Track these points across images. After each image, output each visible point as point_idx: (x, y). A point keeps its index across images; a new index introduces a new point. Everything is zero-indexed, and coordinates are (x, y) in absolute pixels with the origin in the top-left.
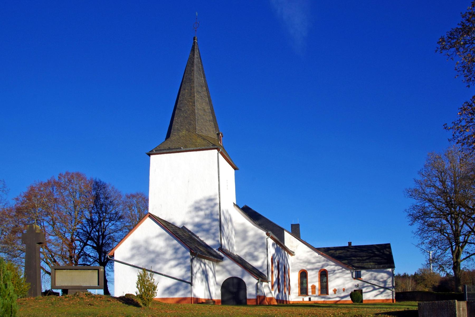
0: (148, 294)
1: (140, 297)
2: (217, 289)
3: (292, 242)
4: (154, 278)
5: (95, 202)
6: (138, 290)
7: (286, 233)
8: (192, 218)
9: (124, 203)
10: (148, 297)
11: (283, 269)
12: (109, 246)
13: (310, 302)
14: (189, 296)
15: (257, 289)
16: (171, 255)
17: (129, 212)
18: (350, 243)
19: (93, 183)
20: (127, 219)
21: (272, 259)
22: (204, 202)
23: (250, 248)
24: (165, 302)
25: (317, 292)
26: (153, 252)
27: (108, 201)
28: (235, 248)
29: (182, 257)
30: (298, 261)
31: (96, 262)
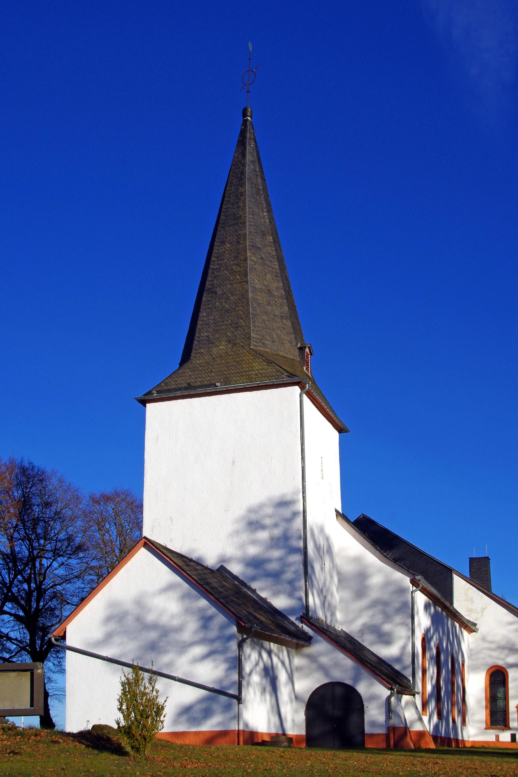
0: (144, 726)
1: (127, 731)
2: (296, 711)
3: (472, 601)
4: (158, 686)
5: (20, 513)
6: (121, 716)
7: (456, 579)
8: (242, 546)
9: (86, 516)
10: (145, 733)
11: (449, 666)
12: (53, 615)
14: (234, 726)
15: (389, 710)
16: (196, 632)
17: (97, 535)
19: (17, 470)
20: (93, 552)
21: (423, 640)
22: (269, 510)
23: (373, 616)
24: (179, 742)
26: (154, 626)
27: (49, 513)
28: (339, 616)
29: (219, 638)
30: (487, 645)
31: (23, 652)
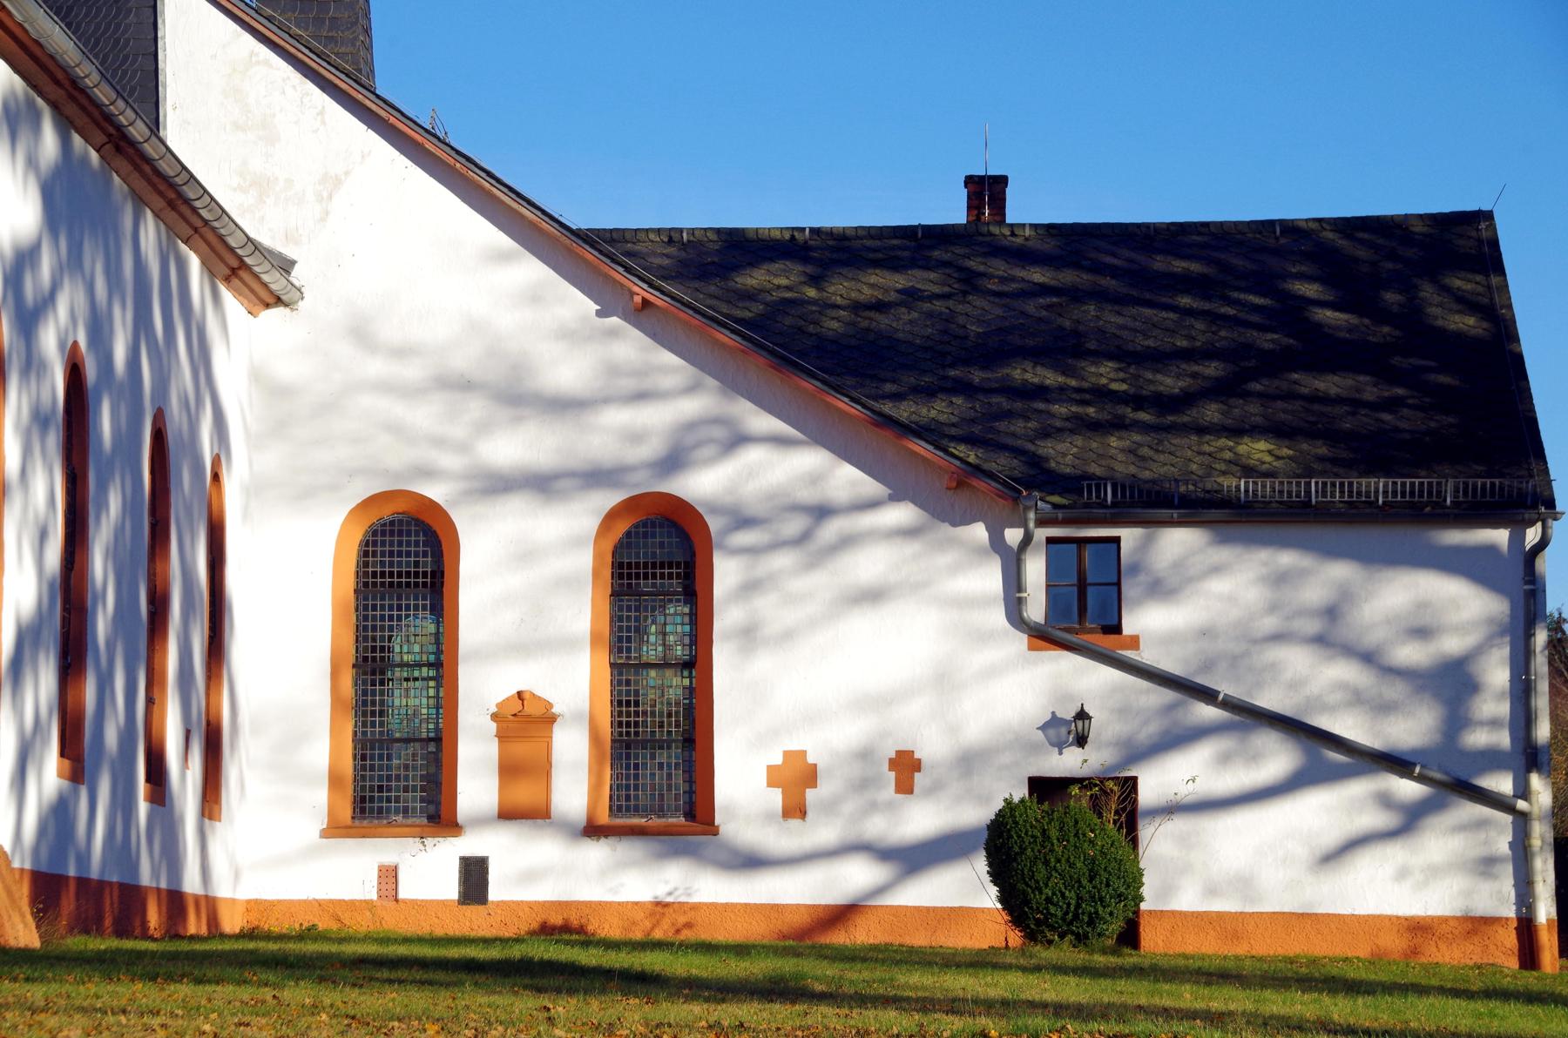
13: (474, 922)
18: (986, 191)
25: (574, 785)
30: (375, 367)
